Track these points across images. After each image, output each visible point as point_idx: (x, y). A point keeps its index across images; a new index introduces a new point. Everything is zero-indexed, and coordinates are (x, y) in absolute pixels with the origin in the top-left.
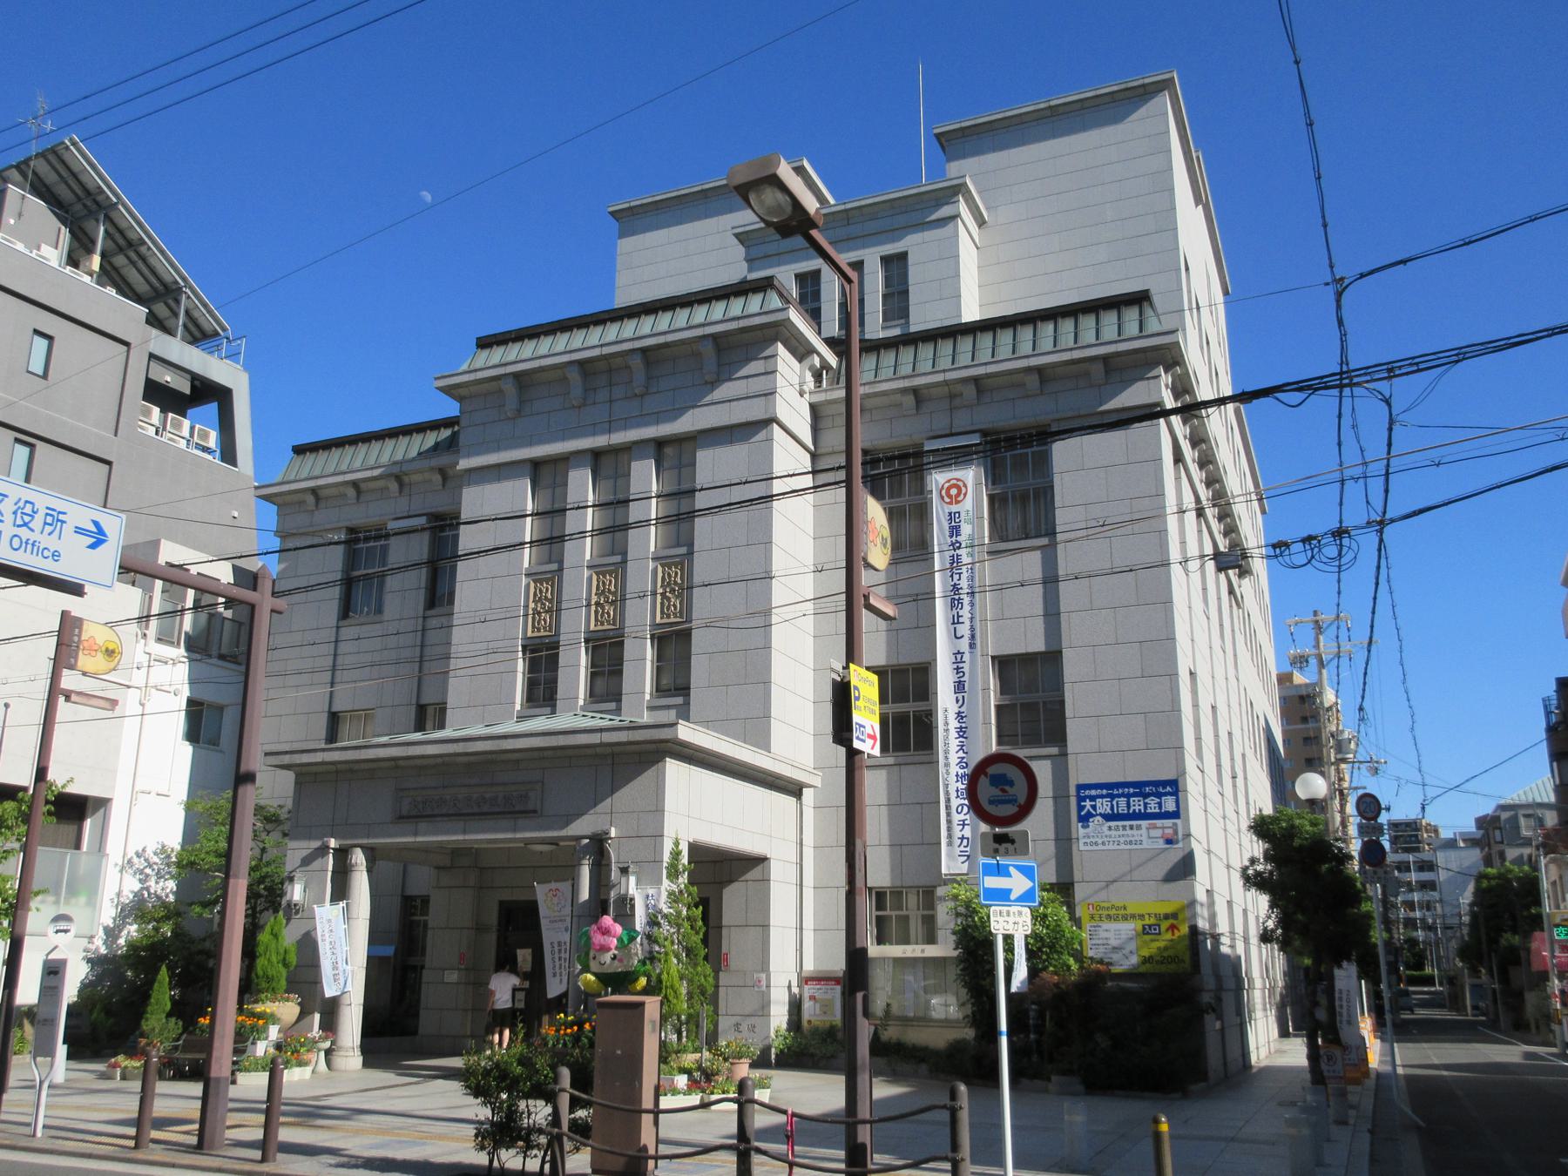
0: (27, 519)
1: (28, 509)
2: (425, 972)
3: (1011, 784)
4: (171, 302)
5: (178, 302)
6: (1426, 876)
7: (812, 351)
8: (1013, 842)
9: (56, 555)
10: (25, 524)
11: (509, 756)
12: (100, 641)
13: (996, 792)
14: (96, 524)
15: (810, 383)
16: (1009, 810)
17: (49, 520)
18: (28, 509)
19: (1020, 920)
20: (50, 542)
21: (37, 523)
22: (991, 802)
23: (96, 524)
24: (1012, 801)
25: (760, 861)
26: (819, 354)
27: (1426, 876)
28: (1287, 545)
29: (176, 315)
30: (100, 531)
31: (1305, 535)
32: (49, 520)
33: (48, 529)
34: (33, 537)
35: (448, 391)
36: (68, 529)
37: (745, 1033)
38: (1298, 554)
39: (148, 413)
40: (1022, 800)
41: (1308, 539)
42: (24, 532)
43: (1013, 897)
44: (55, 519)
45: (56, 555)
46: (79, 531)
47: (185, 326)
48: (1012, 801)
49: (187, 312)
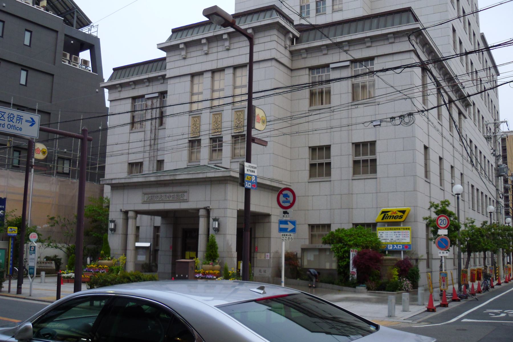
0: (12, 119)
1: (12, 116)
2: (159, 252)
3: (289, 197)
4: (72, 14)
5: (74, 13)
6: (283, 226)
7: (289, 32)
8: (288, 213)
9: (21, 129)
10: (11, 121)
11: (162, 182)
12: (41, 149)
13: (284, 199)
14: (32, 118)
15: (288, 43)
16: (287, 205)
17: (18, 119)
18: (12, 116)
19: (290, 237)
20: (18, 125)
21: (15, 120)
22: (283, 202)
23: (32, 118)
24: (289, 202)
25: (268, 216)
26: (292, 33)
27: (283, 226)
28: (394, 118)
29: (73, 18)
30: (33, 121)
31: (391, 117)
32: (18, 119)
33: (18, 121)
34: (14, 124)
35: (162, 49)
36: (24, 121)
37: (263, 273)
38: (398, 121)
39: (65, 56)
40: (291, 202)
41: (400, 117)
42: (11, 123)
43: (288, 230)
44: (20, 118)
45: (21, 129)
46: (27, 121)
47: (77, 22)
48: (289, 202)
49: (78, 18)
